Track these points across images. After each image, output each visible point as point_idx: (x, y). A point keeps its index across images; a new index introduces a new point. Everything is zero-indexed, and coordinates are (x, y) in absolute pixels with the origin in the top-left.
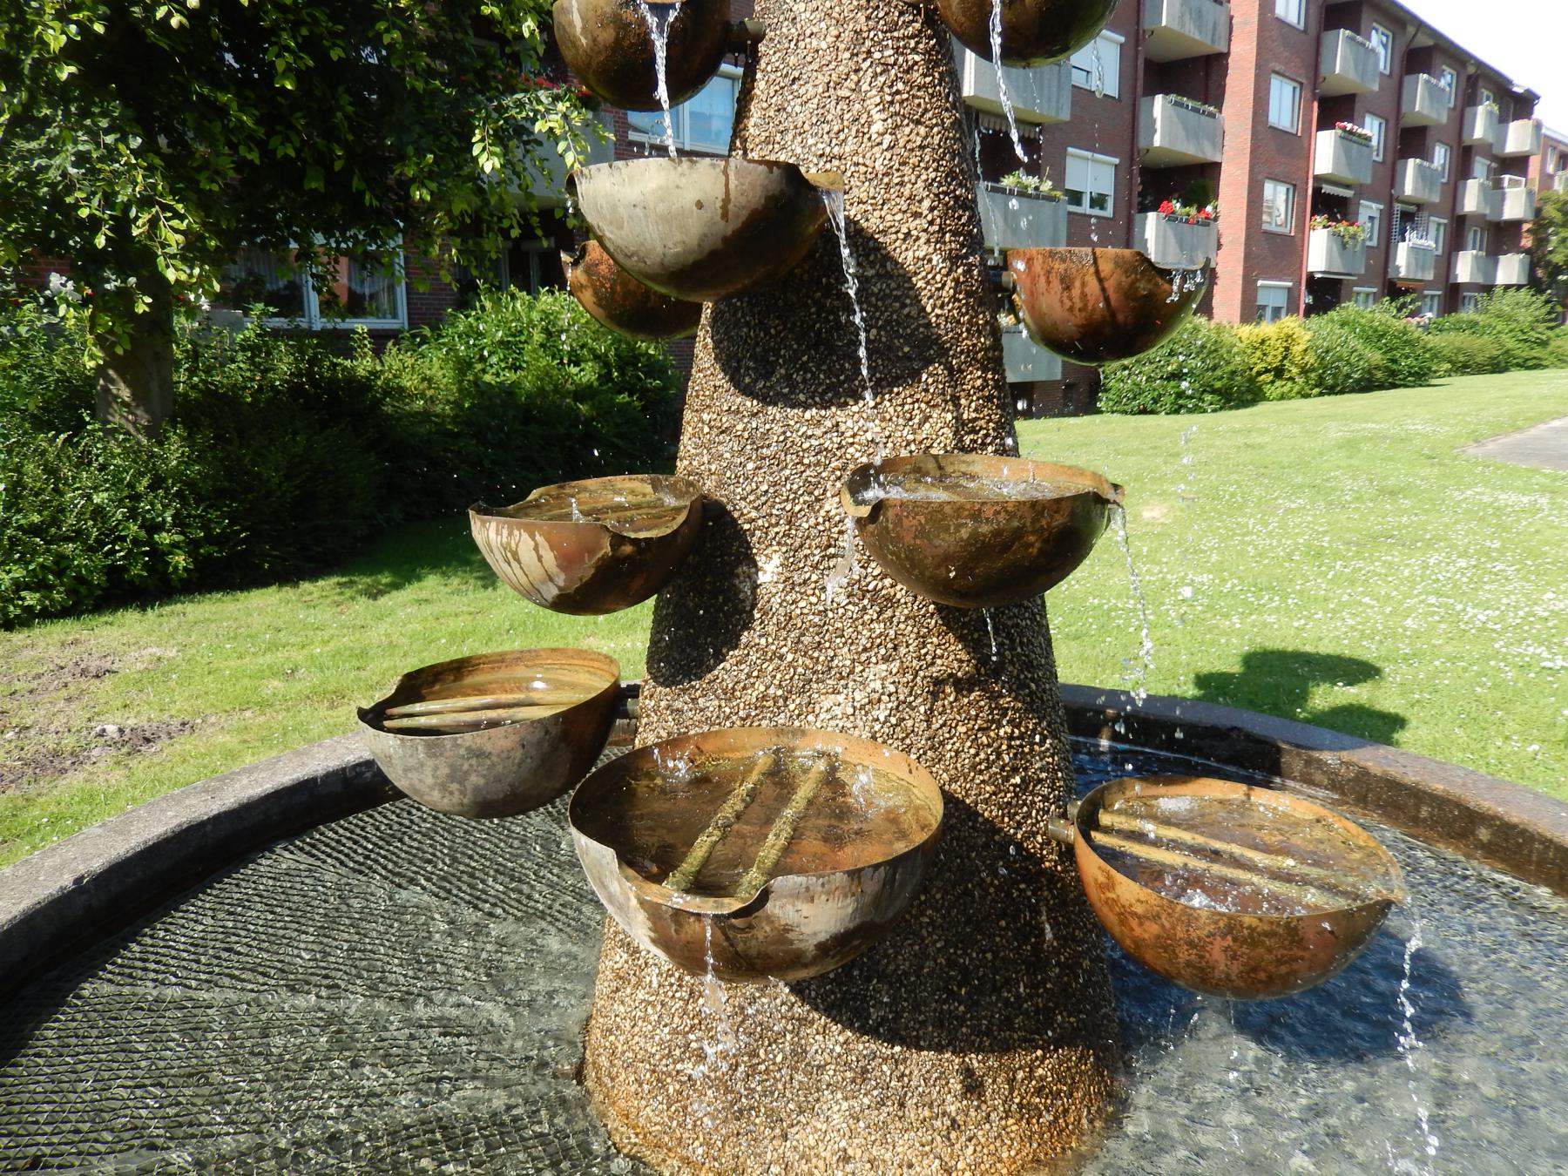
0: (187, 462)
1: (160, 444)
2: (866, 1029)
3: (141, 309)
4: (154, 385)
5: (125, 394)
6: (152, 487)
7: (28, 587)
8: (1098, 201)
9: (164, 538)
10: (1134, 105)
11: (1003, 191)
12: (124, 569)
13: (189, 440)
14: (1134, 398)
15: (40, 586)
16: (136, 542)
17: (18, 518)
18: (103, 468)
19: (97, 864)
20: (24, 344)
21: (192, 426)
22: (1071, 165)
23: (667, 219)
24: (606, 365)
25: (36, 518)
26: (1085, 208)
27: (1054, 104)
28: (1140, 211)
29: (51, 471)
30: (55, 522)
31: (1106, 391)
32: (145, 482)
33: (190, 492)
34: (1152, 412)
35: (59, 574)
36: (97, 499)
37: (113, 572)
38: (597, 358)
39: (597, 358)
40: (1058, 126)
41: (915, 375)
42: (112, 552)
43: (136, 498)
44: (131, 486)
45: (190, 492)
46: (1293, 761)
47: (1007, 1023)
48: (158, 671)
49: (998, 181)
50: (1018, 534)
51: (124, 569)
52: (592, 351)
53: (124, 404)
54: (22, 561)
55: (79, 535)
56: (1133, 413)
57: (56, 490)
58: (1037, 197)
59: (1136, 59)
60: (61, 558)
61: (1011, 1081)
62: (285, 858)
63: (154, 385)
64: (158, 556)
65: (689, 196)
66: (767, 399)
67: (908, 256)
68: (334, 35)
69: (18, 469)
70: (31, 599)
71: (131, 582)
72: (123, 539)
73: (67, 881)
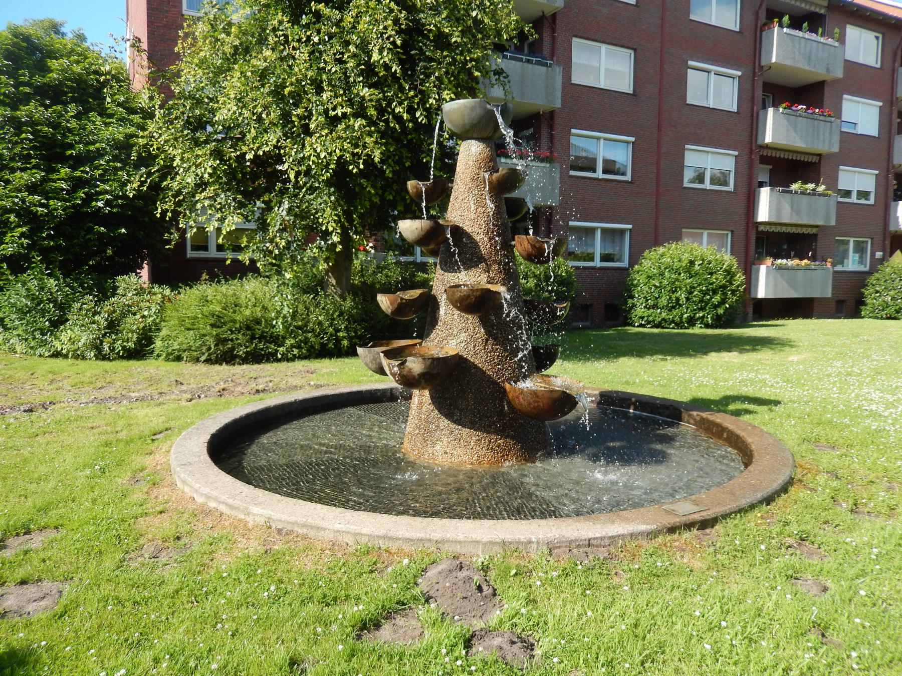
0: (352, 308)
1: (344, 301)
2: (454, 422)
3: (338, 250)
4: (344, 280)
5: (334, 282)
6: (339, 316)
7: (295, 347)
8: (863, 194)
9: (341, 334)
10: (890, 140)
11: (791, 192)
12: (326, 344)
13: (353, 300)
14: (883, 310)
15: (299, 347)
16: (331, 335)
17: (295, 323)
18: (323, 309)
19: (301, 398)
20: (304, 264)
21: (355, 294)
22: (842, 175)
23: (412, 231)
24: (539, 280)
25: (300, 323)
26: (854, 199)
27: (827, 142)
28: (895, 200)
29: (307, 308)
30: (306, 326)
31: (866, 305)
32: (337, 314)
33: (352, 319)
34: (895, 318)
35: (306, 344)
36: (320, 318)
37: (323, 345)
38: (535, 276)
39: (535, 276)
40: (832, 155)
41: (477, 266)
42: (323, 338)
43: (333, 319)
44: (332, 315)
45: (352, 319)
46: (685, 416)
47: (490, 426)
48: (331, 374)
49: (789, 187)
50: (469, 296)
51: (326, 344)
52: (533, 273)
53: (333, 285)
54: (295, 338)
55: (313, 330)
56: (882, 318)
57: (307, 314)
58: (814, 195)
59: (891, 114)
60: (306, 338)
61: (490, 442)
62: (351, 410)
63: (344, 280)
64: (338, 341)
65: (415, 227)
66: (445, 271)
67: (477, 238)
68: (407, 157)
69: (297, 307)
70: (296, 351)
71: (328, 350)
72: (327, 333)
73: (293, 400)
